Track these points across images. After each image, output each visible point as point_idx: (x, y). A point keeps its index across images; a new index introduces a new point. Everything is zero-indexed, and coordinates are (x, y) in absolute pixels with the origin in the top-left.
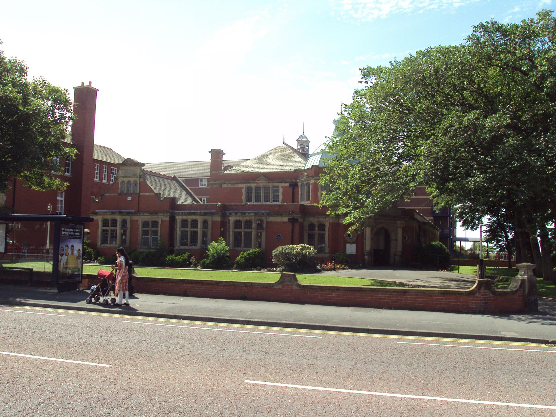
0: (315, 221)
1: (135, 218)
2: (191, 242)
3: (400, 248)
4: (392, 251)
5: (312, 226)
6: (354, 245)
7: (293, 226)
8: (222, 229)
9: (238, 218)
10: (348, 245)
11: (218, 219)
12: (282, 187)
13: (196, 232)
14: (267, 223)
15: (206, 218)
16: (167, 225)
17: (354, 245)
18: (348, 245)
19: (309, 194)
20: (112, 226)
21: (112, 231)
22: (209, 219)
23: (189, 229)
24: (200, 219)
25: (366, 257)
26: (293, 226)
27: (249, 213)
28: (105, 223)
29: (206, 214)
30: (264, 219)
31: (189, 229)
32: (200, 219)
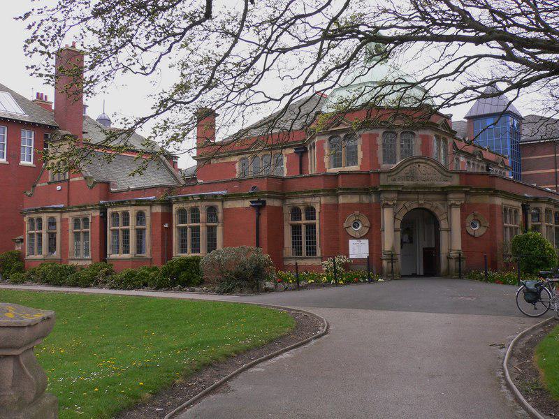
0: (299, 202)
1: (66, 215)
2: (534, 225)
3: (457, 245)
4: (444, 249)
5: (296, 213)
6: (366, 242)
7: (259, 214)
8: (166, 225)
9: (181, 206)
10: (351, 242)
11: (158, 209)
12: (286, 155)
13: (313, 226)
14: (225, 210)
15: (141, 208)
16: (97, 222)
17: (366, 242)
18: (351, 242)
19: (311, 158)
20: (307, 219)
21: (308, 226)
22: (147, 210)
23: (304, 221)
24: (132, 211)
25: (385, 263)
26: (259, 214)
27: (192, 197)
28: (76, 223)
29: (139, 203)
30: (219, 204)
31: (304, 221)
32: (318, 203)
